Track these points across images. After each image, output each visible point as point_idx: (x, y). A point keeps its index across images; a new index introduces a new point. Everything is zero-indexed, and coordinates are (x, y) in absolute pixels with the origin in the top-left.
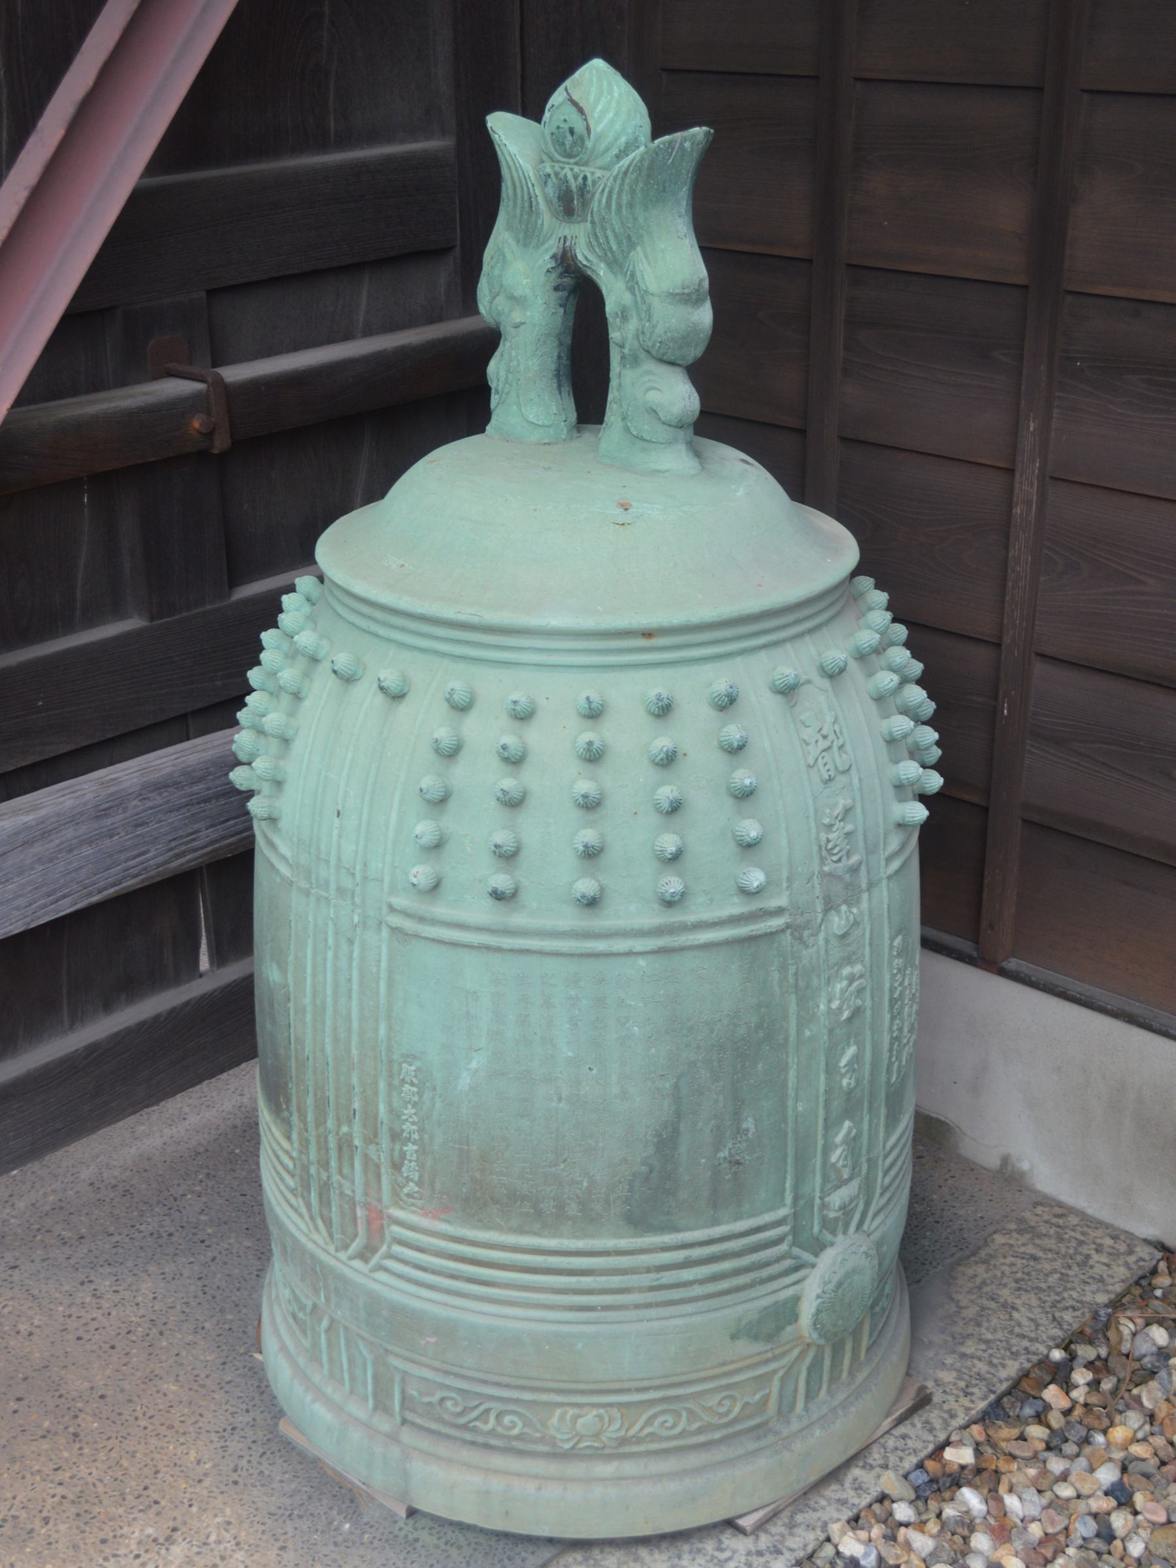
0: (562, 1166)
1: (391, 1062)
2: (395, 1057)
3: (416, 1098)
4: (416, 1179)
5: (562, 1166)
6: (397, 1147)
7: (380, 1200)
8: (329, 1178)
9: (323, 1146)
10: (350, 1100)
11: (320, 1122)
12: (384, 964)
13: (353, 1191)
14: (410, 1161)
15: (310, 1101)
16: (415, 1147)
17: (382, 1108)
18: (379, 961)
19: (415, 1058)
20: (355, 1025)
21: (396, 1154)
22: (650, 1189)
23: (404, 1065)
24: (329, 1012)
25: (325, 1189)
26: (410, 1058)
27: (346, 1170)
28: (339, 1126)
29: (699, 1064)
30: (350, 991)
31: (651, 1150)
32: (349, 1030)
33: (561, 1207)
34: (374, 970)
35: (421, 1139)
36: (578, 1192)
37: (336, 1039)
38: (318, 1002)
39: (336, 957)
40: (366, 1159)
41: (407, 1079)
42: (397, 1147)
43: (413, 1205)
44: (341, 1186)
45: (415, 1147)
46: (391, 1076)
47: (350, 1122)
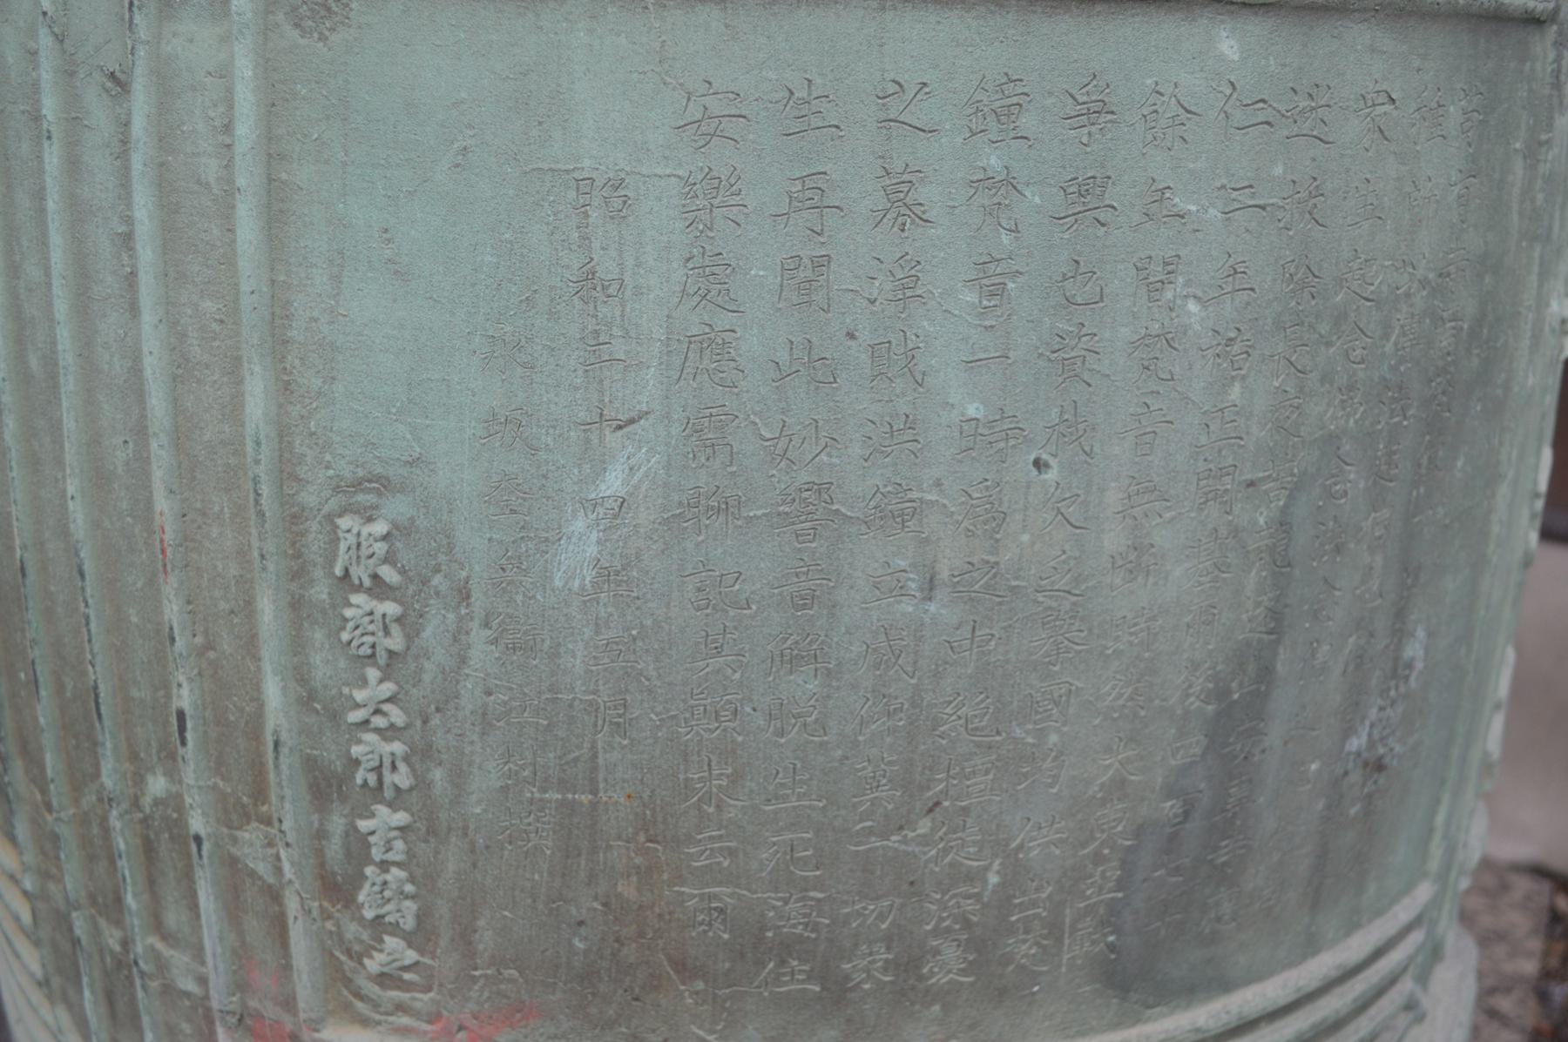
0: (924, 826)
1: (295, 518)
2: (309, 498)
3: (396, 642)
4: (409, 923)
5: (924, 826)
6: (337, 824)
7: (289, 1004)
8: (126, 943)
9: (98, 852)
10: (164, 686)
11: (82, 776)
12: (246, 130)
13: (203, 981)
14: (384, 866)
15: (45, 712)
16: (401, 818)
17: (273, 691)
18: (228, 128)
19: (384, 485)
20: (158, 404)
21: (334, 849)
22: (1177, 871)
23: (344, 523)
24: (69, 384)
25: (119, 976)
26: (365, 488)
27: (174, 917)
28: (139, 780)
29: (1347, 447)
30: (131, 280)
31: (1196, 743)
32: (141, 432)
33: (909, 965)
34: (211, 169)
35: (422, 783)
36: (969, 906)
37: (100, 479)
38: (34, 362)
39: (73, 166)
40: (234, 872)
41: (360, 573)
42: (337, 824)
43: (400, 1008)
44: (162, 966)
45: (401, 818)
46: (299, 573)
47: (170, 761)
